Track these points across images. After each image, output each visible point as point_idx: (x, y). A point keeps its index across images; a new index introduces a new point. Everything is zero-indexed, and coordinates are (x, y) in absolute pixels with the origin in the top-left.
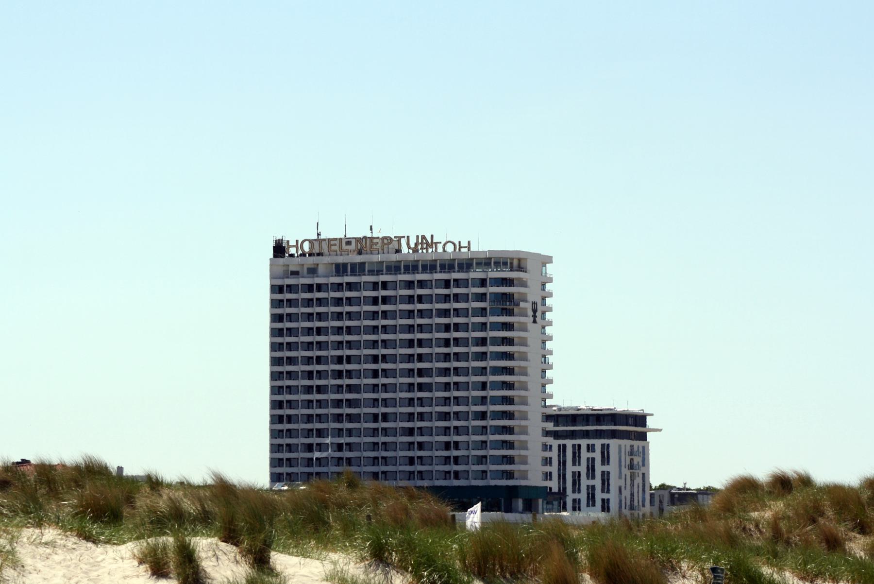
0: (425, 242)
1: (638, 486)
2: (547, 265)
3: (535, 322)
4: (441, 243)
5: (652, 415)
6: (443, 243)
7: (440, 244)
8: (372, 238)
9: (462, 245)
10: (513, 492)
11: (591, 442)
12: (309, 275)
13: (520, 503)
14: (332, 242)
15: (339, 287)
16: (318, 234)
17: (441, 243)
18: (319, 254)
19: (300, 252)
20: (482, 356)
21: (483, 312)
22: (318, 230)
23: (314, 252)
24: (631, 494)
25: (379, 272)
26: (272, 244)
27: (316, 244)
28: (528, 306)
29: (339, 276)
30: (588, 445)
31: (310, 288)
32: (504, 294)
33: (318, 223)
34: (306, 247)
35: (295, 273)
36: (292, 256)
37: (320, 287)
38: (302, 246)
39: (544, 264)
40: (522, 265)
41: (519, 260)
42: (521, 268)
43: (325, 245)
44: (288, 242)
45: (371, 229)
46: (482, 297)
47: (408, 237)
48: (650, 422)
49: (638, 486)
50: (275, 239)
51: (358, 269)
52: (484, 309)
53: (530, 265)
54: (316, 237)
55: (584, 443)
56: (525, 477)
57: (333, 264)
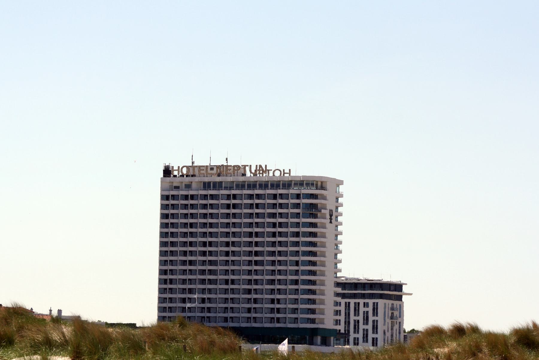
0: (262, 170)
1: (396, 330)
2: (340, 186)
3: (331, 222)
4: (271, 170)
5: (406, 284)
6: (273, 171)
7: (271, 171)
8: (227, 166)
9: (285, 172)
10: (314, 332)
11: (366, 301)
12: (186, 189)
13: (319, 339)
14: (201, 168)
15: (205, 197)
16: (193, 163)
17: (271, 170)
18: (192, 176)
19: (180, 174)
20: (297, 244)
21: (297, 215)
22: (192, 159)
23: (189, 174)
24: (391, 335)
25: (231, 188)
26: (162, 168)
27: (191, 169)
28: (327, 212)
29: (205, 190)
30: (364, 303)
31: (186, 197)
32: (311, 204)
33: (192, 155)
34: (185, 171)
35: (177, 188)
36: (175, 176)
37: (193, 197)
38: (251, 170)
39: (338, 186)
40: (324, 186)
41: (322, 182)
42: (323, 188)
43: (196, 170)
44: (173, 167)
45: (227, 160)
46: (297, 206)
47: (251, 166)
48: (405, 289)
49: (396, 330)
50: (164, 165)
51: (218, 185)
52: (299, 214)
53: (328, 186)
54: (191, 165)
55: (361, 301)
56: (322, 321)
57: (201, 182)
